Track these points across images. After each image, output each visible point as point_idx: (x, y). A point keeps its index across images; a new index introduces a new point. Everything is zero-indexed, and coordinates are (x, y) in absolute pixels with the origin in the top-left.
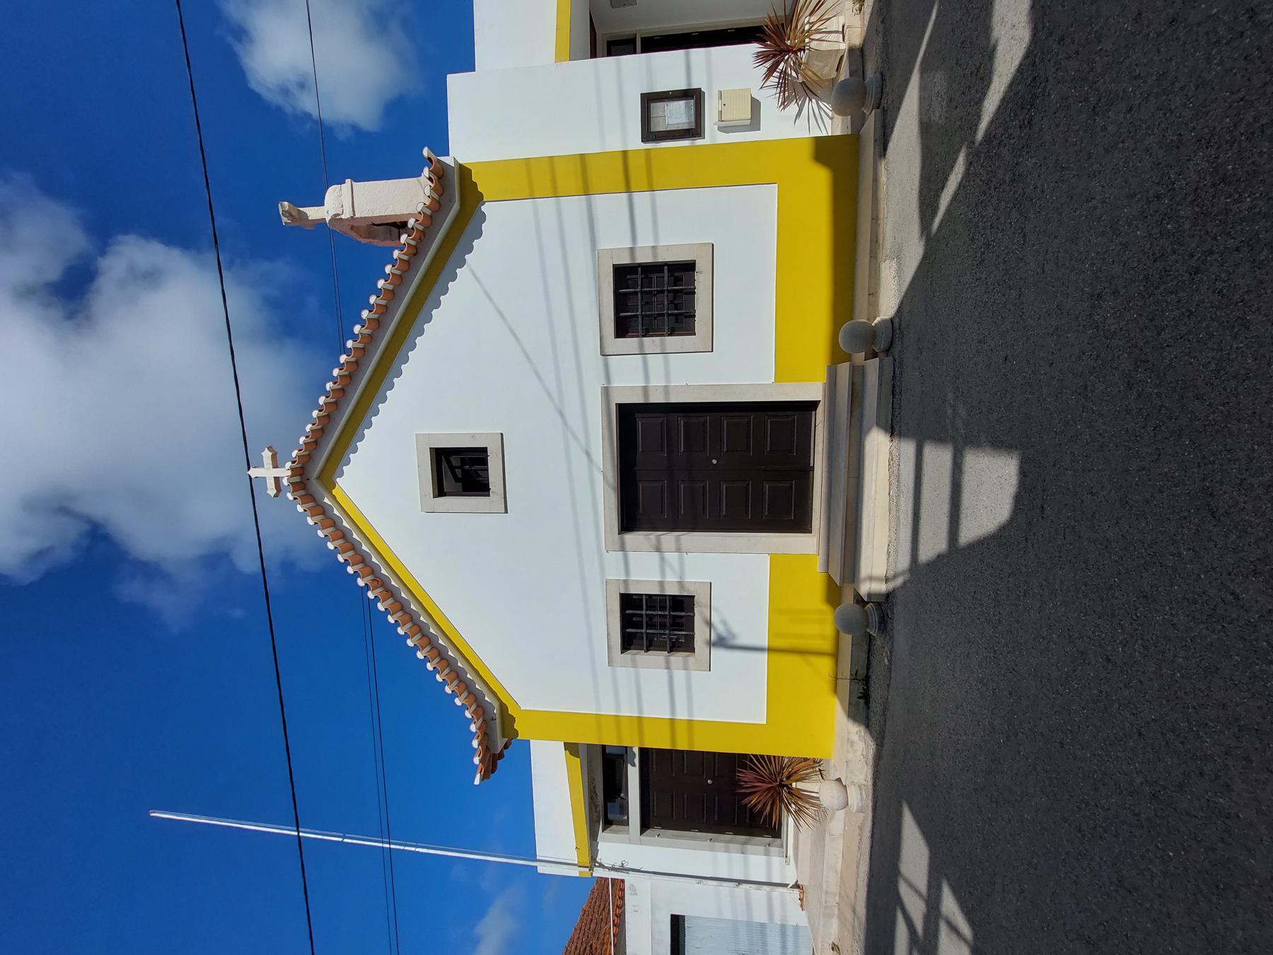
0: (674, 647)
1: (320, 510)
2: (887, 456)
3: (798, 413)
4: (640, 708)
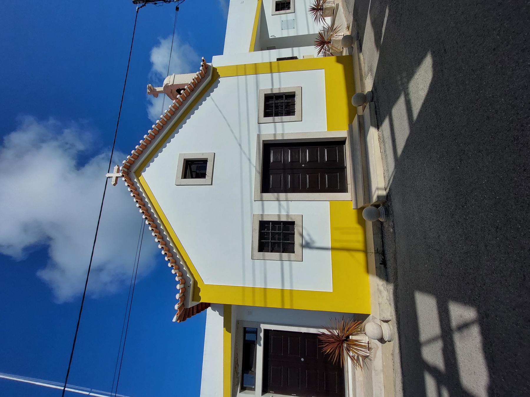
1: (132, 185)
2: (377, 137)
3: (341, 142)
4: (266, 283)
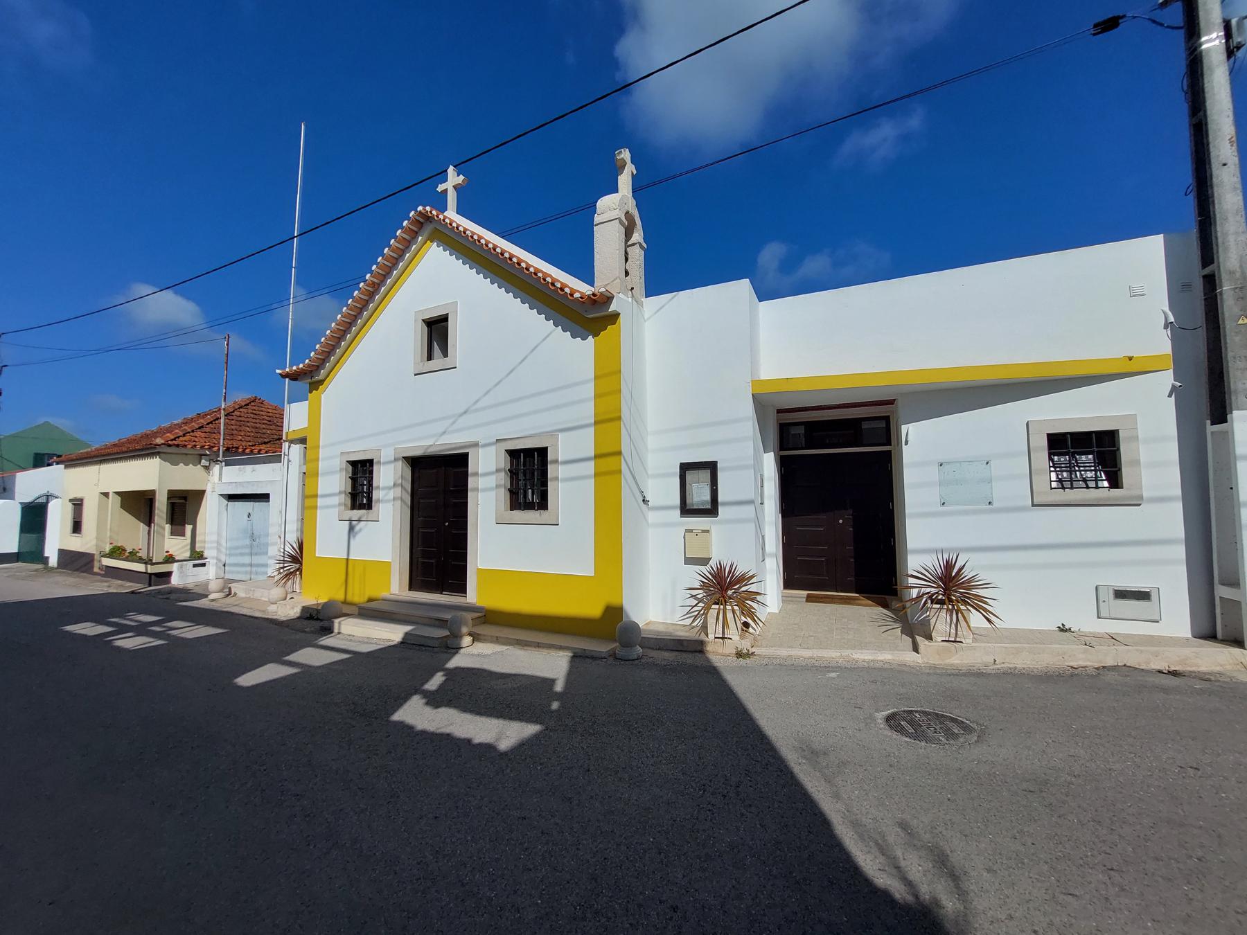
0: (513, 493)
3: (461, 589)
